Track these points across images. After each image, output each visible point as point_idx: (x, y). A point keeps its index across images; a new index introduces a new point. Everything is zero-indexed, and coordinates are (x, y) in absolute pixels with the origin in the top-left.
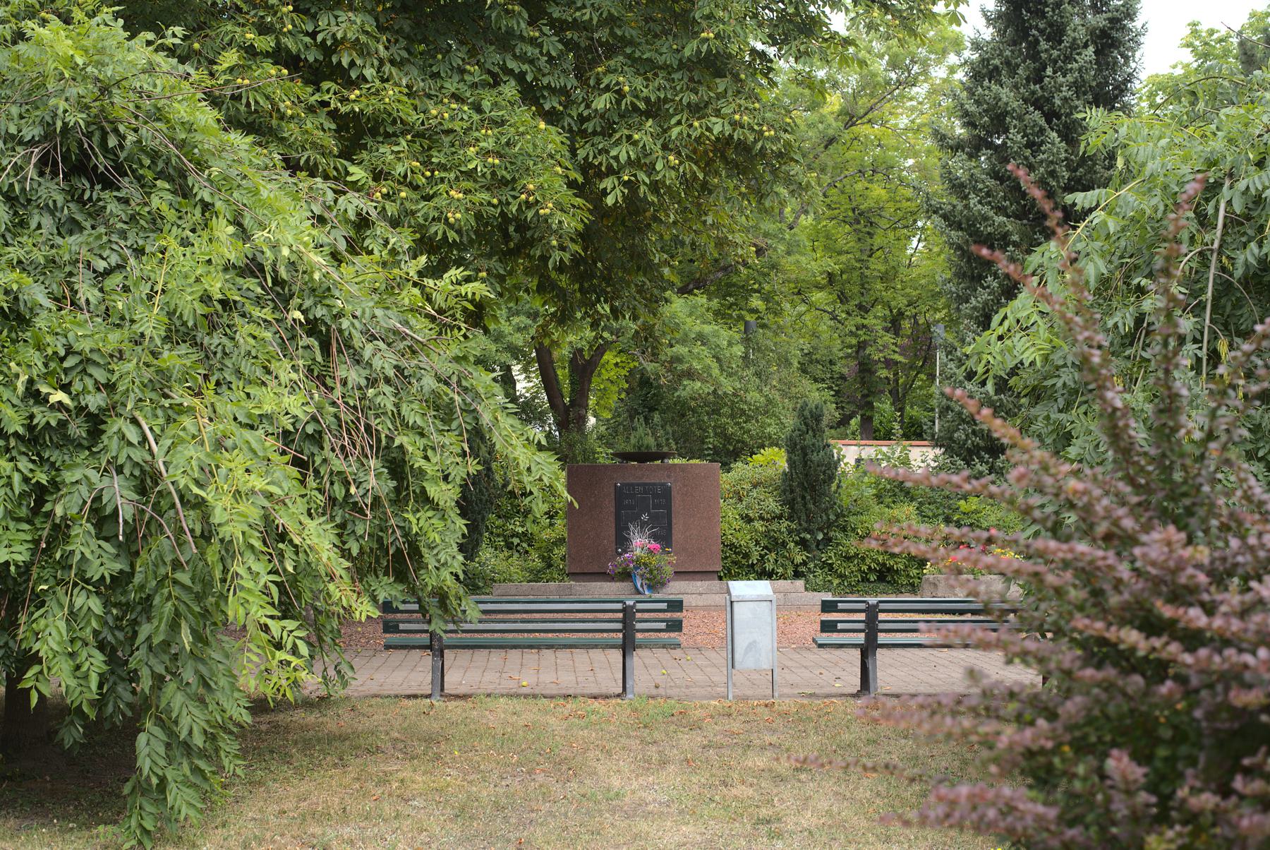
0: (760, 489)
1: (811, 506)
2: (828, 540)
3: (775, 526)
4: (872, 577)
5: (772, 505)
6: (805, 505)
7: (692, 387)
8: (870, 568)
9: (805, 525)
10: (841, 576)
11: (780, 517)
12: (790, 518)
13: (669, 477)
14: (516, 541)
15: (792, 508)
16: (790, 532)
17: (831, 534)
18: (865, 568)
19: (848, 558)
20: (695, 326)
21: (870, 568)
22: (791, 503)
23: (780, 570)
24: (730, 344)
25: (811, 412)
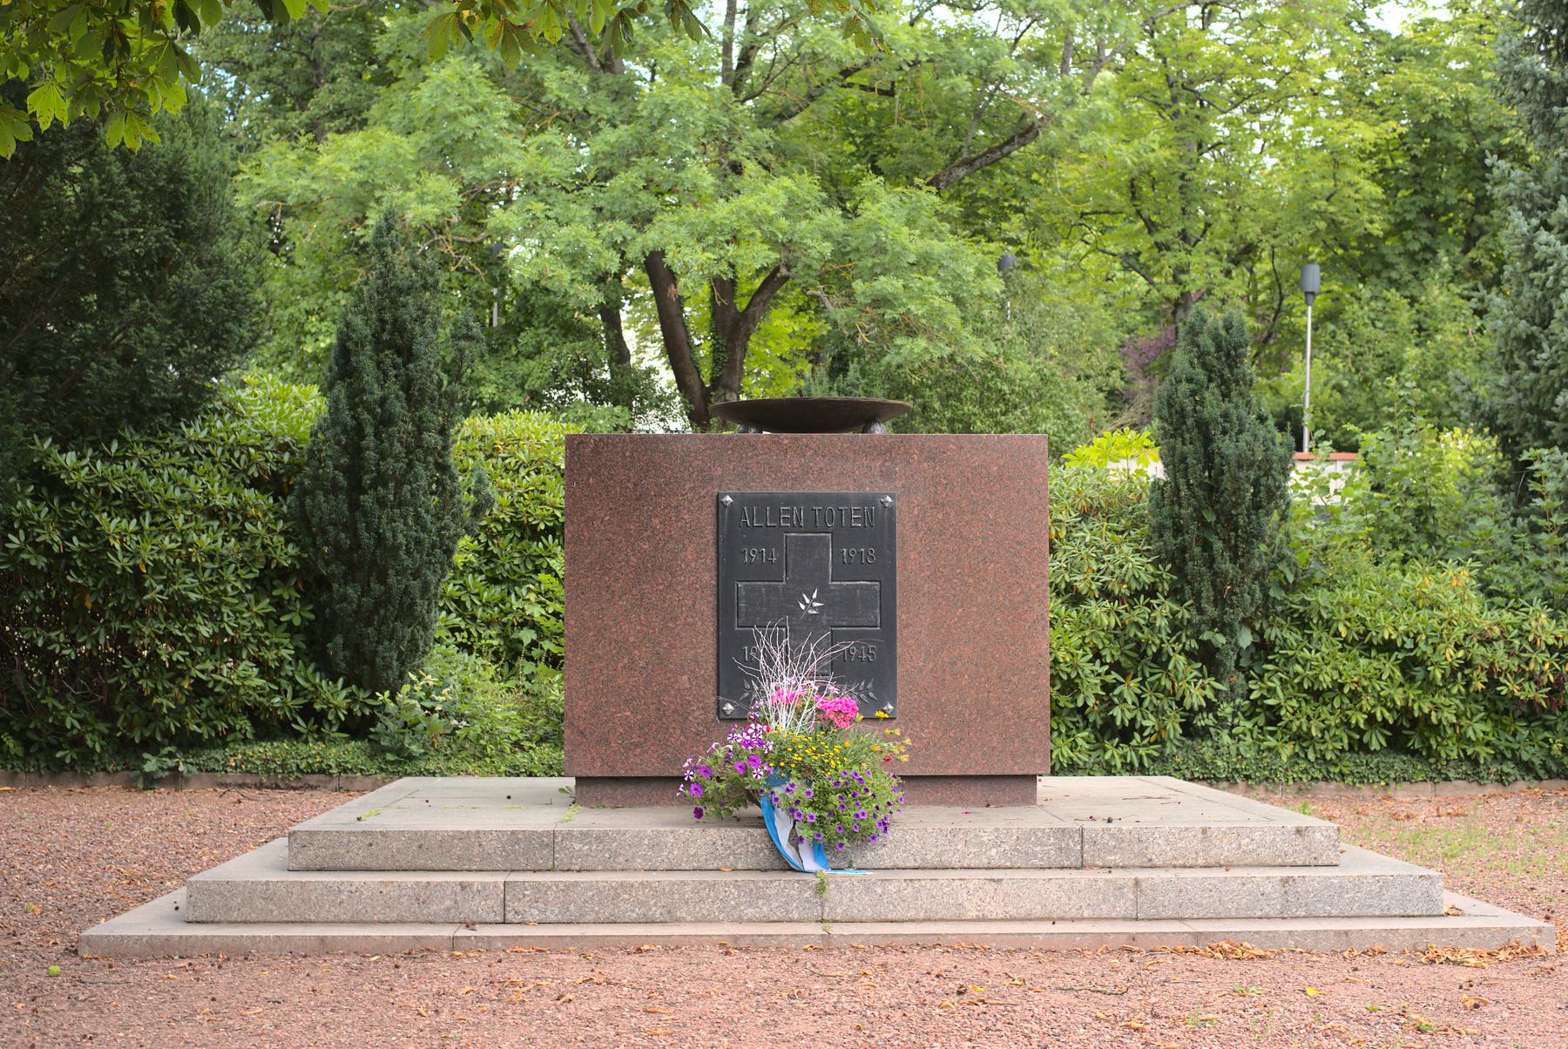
0: (1099, 523)
1: (1227, 566)
2: (1263, 648)
3: (1140, 614)
4: (1376, 741)
5: (1135, 565)
6: (1210, 562)
7: (912, 348)
8: (1371, 719)
9: (1212, 611)
10: (1301, 738)
11: (1151, 592)
12: (1175, 594)
13: (887, 475)
14: (527, 636)
15: (1179, 570)
16: (1176, 627)
17: (1272, 633)
18: (1359, 719)
19: (1316, 694)
20: (913, 244)
21: (1371, 719)
22: (1177, 559)
23: (1150, 722)
24: (980, 274)
25: (1216, 338)
